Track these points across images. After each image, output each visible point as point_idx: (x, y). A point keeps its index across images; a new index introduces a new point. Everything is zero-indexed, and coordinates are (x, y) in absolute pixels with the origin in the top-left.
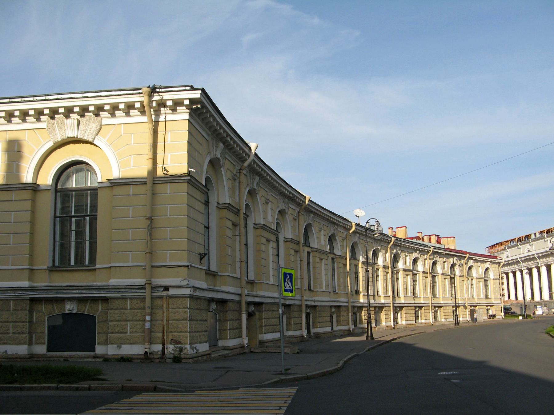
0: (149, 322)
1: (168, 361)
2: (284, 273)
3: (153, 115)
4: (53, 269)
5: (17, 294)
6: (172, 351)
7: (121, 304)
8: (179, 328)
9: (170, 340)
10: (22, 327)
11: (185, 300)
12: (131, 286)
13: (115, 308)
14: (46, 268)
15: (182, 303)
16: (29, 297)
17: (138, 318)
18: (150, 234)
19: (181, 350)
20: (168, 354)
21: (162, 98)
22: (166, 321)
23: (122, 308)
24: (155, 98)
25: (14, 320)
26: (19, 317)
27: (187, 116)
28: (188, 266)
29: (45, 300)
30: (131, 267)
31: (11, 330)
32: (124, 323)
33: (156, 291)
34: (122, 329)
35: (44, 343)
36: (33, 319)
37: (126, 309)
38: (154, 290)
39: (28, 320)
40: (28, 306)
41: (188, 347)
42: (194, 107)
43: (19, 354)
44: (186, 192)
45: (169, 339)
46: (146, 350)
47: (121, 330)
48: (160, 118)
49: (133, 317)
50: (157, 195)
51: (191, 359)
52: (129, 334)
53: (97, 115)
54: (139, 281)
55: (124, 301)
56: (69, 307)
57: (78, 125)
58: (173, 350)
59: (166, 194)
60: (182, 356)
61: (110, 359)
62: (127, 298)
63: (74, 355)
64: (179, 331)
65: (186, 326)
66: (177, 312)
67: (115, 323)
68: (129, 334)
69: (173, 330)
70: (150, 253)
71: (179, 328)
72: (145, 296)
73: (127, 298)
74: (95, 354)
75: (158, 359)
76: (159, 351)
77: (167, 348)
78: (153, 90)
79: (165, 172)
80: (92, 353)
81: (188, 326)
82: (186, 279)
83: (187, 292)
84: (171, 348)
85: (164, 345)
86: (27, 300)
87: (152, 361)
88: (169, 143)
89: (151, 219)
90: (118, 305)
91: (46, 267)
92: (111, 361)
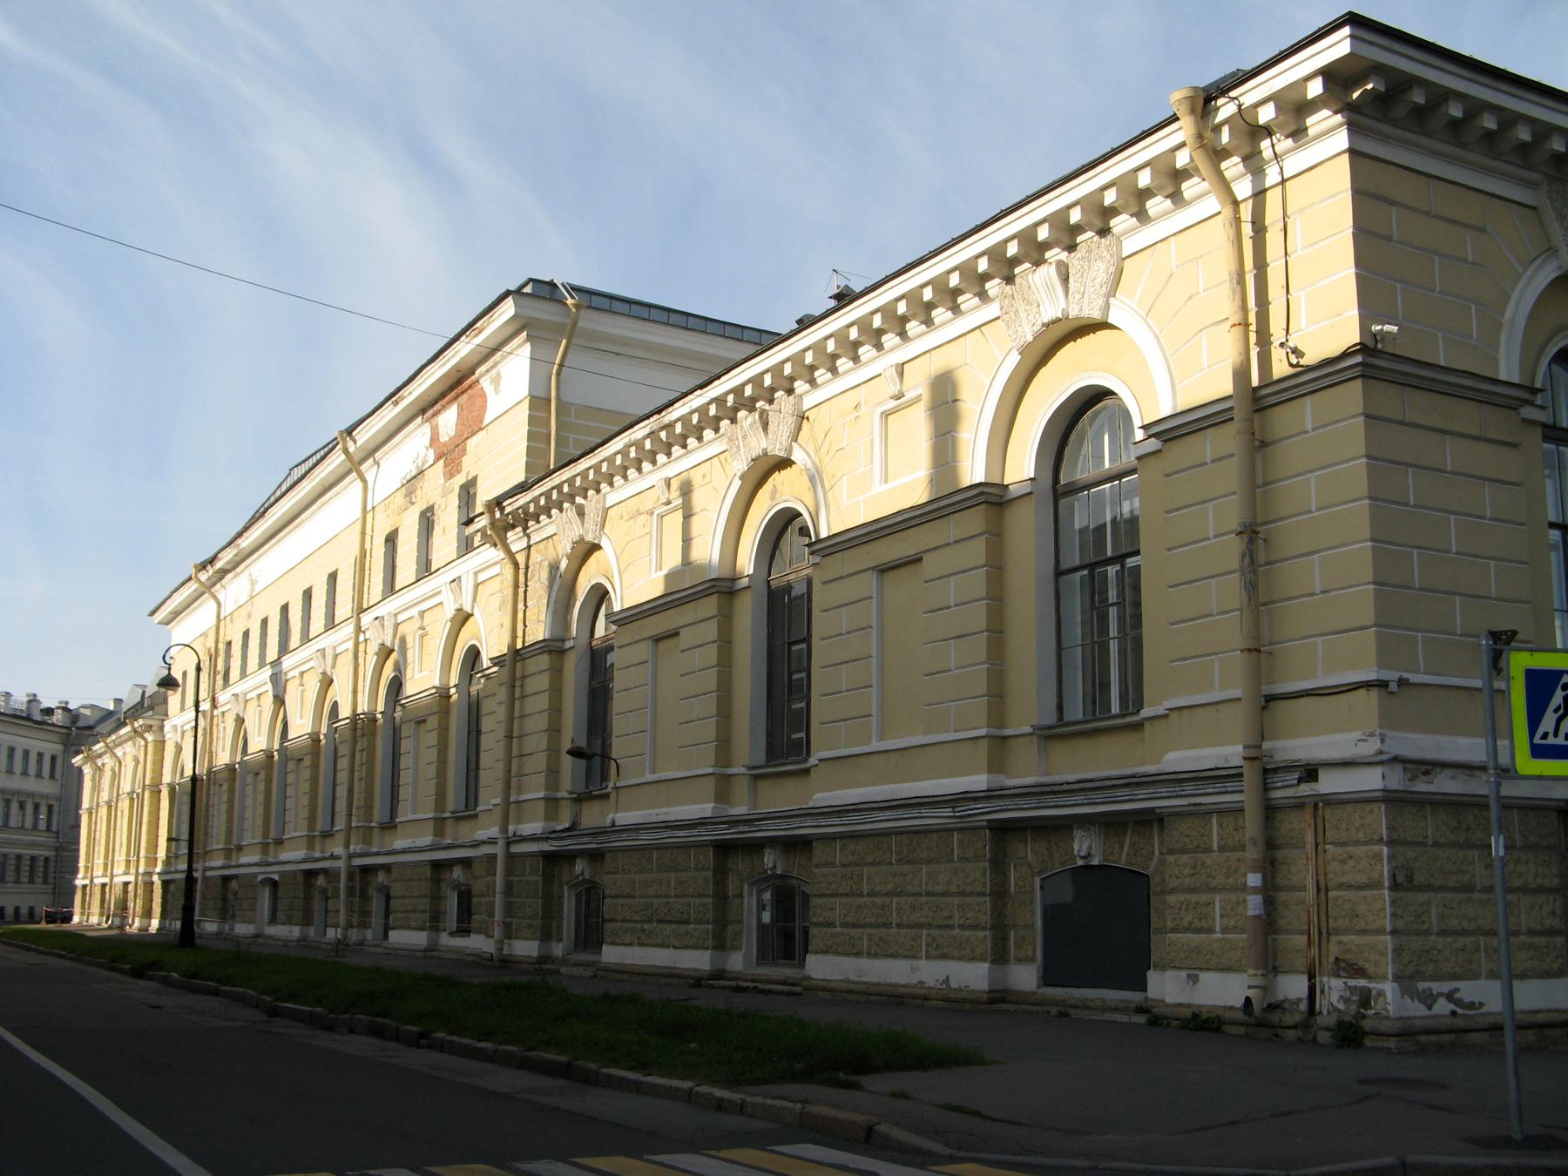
0: (1255, 894)
1: (1324, 1037)
2: (1531, 675)
4: (1049, 735)
5: (961, 810)
6: (1339, 1001)
7: (1195, 833)
8: (1357, 916)
9: (1332, 960)
10: (977, 908)
11: (1371, 811)
12: (1217, 769)
13: (1179, 846)
14: (1031, 730)
15: (1363, 825)
16: (988, 821)
17: (1239, 882)
18: (1248, 586)
19: (1365, 999)
20: (1325, 1013)
22: (1319, 890)
23: (1198, 846)
24: (1222, 115)
25: (960, 890)
26: (972, 878)
27: (1341, 140)
28: (1382, 685)
29: (1033, 828)
30: (1219, 707)
31: (957, 920)
32: (1204, 898)
33: (1280, 784)
34: (1200, 920)
35: (1032, 959)
36: (1010, 886)
37: (1208, 850)
38: (1275, 780)
39: (988, 887)
41: (1389, 988)
42: (1355, 95)
43: (971, 988)
44: (1358, 415)
45: (1327, 957)
46: (1250, 993)
47: (1197, 921)
48: (1267, 178)
49: (1227, 878)
50: (1279, 445)
51: (1395, 1038)
52: (1219, 935)
53: (1104, 232)
54: (1231, 753)
55: (1202, 823)
56: (1085, 847)
57: (1065, 279)
58: (1341, 997)
59: (1304, 436)
60: (1367, 1024)
61: (1167, 1018)
62: (1210, 813)
63: (1092, 1000)
64: (1357, 928)
65: (1380, 910)
66: (1351, 857)
67: (1181, 897)
68: (1219, 935)
69: (1341, 923)
70: (1255, 650)
71: (1357, 916)
72: (1486, 800)
73: (1210, 813)
74: (1146, 998)
75: (1295, 1027)
76: (1300, 1000)
77: (1322, 992)
78: (1205, 100)
79: (1294, 360)
80: (1134, 997)
81: (1384, 909)
82: (1372, 735)
83: (1370, 780)
84: (1335, 990)
85: (1311, 977)
86: (982, 828)
87: (1276, 1035)
88: (1300, 253)
89: (1251, 533)
90: (1188, 836)
91: (1028, 729)
92: (1169, 1024)
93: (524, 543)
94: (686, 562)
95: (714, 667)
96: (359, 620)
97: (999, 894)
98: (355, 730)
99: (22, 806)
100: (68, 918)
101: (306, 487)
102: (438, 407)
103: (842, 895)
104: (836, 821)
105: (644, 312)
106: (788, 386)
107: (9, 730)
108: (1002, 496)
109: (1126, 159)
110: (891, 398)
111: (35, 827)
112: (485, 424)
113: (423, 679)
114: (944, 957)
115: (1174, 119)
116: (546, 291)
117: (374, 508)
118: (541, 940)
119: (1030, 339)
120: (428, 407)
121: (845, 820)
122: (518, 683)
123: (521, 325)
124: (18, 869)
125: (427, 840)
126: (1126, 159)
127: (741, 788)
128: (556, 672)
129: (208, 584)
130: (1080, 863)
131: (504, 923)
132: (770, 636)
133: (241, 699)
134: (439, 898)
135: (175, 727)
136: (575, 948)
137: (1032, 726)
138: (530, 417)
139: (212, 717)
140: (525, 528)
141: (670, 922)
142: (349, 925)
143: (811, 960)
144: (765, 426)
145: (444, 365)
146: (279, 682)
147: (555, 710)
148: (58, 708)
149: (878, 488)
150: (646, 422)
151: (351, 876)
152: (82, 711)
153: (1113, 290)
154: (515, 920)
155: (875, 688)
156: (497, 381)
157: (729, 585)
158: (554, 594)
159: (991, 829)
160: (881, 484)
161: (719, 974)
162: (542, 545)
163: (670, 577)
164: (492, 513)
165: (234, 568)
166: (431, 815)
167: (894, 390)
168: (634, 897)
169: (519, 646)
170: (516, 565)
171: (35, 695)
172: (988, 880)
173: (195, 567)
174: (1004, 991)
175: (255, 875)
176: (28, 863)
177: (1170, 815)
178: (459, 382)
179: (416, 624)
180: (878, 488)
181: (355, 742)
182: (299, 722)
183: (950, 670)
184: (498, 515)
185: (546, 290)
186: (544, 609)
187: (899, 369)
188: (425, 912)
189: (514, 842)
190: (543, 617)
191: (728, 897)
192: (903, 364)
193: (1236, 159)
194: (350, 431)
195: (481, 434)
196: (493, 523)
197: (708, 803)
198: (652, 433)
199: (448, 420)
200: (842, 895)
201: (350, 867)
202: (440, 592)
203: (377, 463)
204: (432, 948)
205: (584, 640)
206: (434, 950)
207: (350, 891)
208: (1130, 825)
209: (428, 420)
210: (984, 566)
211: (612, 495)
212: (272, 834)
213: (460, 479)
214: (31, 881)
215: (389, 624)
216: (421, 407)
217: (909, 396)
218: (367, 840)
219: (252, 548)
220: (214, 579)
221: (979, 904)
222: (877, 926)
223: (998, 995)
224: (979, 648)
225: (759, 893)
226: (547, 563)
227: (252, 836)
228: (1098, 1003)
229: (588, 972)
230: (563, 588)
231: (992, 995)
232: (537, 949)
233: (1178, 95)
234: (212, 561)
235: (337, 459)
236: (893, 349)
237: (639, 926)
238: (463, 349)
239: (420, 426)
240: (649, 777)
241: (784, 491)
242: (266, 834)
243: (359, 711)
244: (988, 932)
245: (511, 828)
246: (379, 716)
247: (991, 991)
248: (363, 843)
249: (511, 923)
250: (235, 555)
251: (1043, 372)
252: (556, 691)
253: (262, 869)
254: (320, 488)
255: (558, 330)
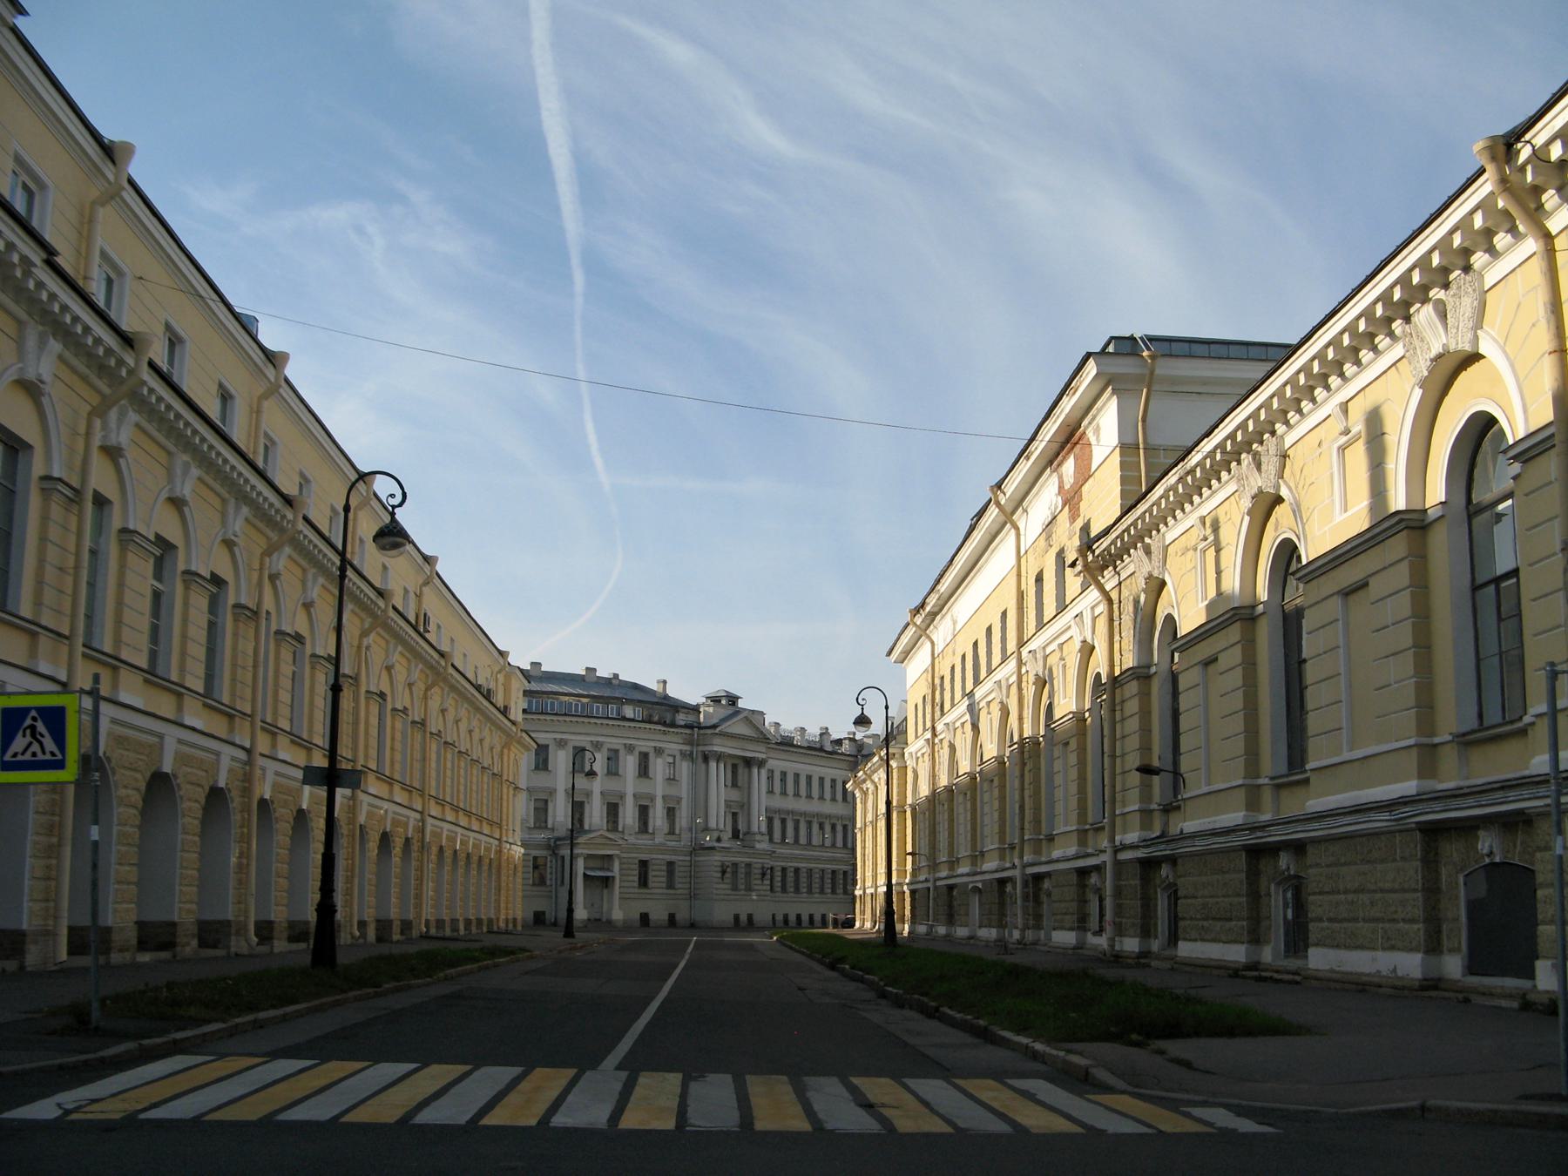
3: (272, 947)
14: (1450, 738)
16: (1417, 823)
21: (1533, 147)
35: (1458, 950)
39: (1420, 885)
40: (1419, 848)
78: (1506, 146)
86: (1411, 830)
93: (1115, 582)
94: (1219, 593)
95: (1410, 648)
96: (1020, 654)
97: (1432, 890)
98: (1023, 753)
99: (821, 827)
100: (850, 923)
101: (978, 536)
102: (1060, 458)
103: (1327, 893)
104: (1316, 825)
105: (1223, 350)
106: (1271, 429)
107: (817, 763)
108: (1423, 520)
109: (1461, 205)
110: (1341, 434)
111: (834, 845)
112: (1093, 470)
113: (1066, 704)
114: (1393, 948)
115: (1482, 171)
116: (1127, 347)
117: (1026, 552)
118: (1142, 937)
119: (1426, 373)
120: (1052, 460)
121: (1323, 824)
122: (1118, 708)
123: (1107, 381)
124: (822, 878)
125: (1072, 851)
126: (1461, 205)
127: (1267, 796)
128: (1145, 695)
129: (923, 627)
130: (1487, 860)
131: (1114, 923)
132: (1286, 656)
133: (951, 728)
134: (1086, 902)
135: (911, 754)
136: (1169, 944)
137: (1451, 734)
138: (1122, 463)
139: (934, 744)
140: (1115, 567)
141: (1220, 919)
142: (1026, 927)
143: (1313, 952)
144: (1259, 467)
145: (1055, 421)
146: (973, 709)
147: (1146, 730)
148: (845, 739)
149: (1339, 517)
150: (1176, 469)
151: (1025, 884)
152: (865, 740)
153: (1478, 324)
154: (1124, 920)
155: (1344, 703)
156: (1097, 431)
157: (1248, 611)
158: (1138, 626)
159: (1420, 830)
160: (1341, 514)
161: (1254, 966)
162: (1128, 581)
163: (1209, 607)
164: (1085, 557)
165: (941, 610)
166: (1074, 828)
167: (1341, 427)
168: (1196, 897)
169: (1117, 673)
170: (1110, 601)
171: (827, 729)
172: (1420, 877)
173: (910, 611)
174: (1440, 979)
175: (966, 884)
176: (830, 876)
177: (1539, 815)
178: (1072, 435)
179: (1057, 656)
180: (1339, 517)
181: (1024, 764)
182: (990, 746)
183: (1389, 685)
184: (1090, 558)
185: (1126, 346)
186: (1132, 639)
187: (1344, 407)
188: (1073, 914)
189: (1120, 850)
190: (1131, 648)
191: (1260, 896)
192: (1347, 402)
193: (1552, 192)
194: (999, 486)
195: (1091, 481)
196: (1086, 566)
197: (1408, 779)
198: (1181, 478)
199: (1069, 467)
200: (1327, 893)
201: (1023, 874)
202: (1070, 627)
203: (1025, 511)
204: (1080, 946)
205: (1165, 666)
206: (1081, 948)
207: (1026, 898)
208: (1521, 824)
209: (1055, 470)
210: (1408, 587)
211: (1171, 532)
212: (1044, 830)
213: (1079, 523)
214: (834, 892)
215: (1039, 656)
216: (1048, 460)
217: (1354, 431)
218: (1037, 852)
219: (950, 592)
220: (928, 622)
221: (1414, 900)
222: (1349, 920)
223: (1430, 983)
224: (1406, 665)
225: (1285, 892)
226: (1132, 598)
227: (964, 851)
228: (1499, 991)
229: (1167, 965)
230: (1145, 618)
231: (1425, 983)
232: (1137, 944)
233: (1479, 145)
234: (923, 605)
235: (993, 512)
236: (1338, 389)
237: (1201, 923)
238: (1067, 404)
239: (1050, 476)
240: (1205, 789)
241: (1280, 526)
242: (1002, 840)
243: (1025, 736)
244: (1421, 926)
245: (1118, 838)
246: (1041, 739)
247: (1425, 980)
248: (1034, 854)
249: (1121, 923)
250: (938, 599)
251: (1447, 400)
252: (1145, 713)
253: (971, 879)
254: (988, 537)
255: (1138, 379)
